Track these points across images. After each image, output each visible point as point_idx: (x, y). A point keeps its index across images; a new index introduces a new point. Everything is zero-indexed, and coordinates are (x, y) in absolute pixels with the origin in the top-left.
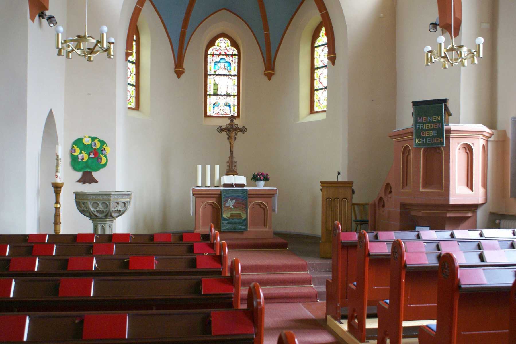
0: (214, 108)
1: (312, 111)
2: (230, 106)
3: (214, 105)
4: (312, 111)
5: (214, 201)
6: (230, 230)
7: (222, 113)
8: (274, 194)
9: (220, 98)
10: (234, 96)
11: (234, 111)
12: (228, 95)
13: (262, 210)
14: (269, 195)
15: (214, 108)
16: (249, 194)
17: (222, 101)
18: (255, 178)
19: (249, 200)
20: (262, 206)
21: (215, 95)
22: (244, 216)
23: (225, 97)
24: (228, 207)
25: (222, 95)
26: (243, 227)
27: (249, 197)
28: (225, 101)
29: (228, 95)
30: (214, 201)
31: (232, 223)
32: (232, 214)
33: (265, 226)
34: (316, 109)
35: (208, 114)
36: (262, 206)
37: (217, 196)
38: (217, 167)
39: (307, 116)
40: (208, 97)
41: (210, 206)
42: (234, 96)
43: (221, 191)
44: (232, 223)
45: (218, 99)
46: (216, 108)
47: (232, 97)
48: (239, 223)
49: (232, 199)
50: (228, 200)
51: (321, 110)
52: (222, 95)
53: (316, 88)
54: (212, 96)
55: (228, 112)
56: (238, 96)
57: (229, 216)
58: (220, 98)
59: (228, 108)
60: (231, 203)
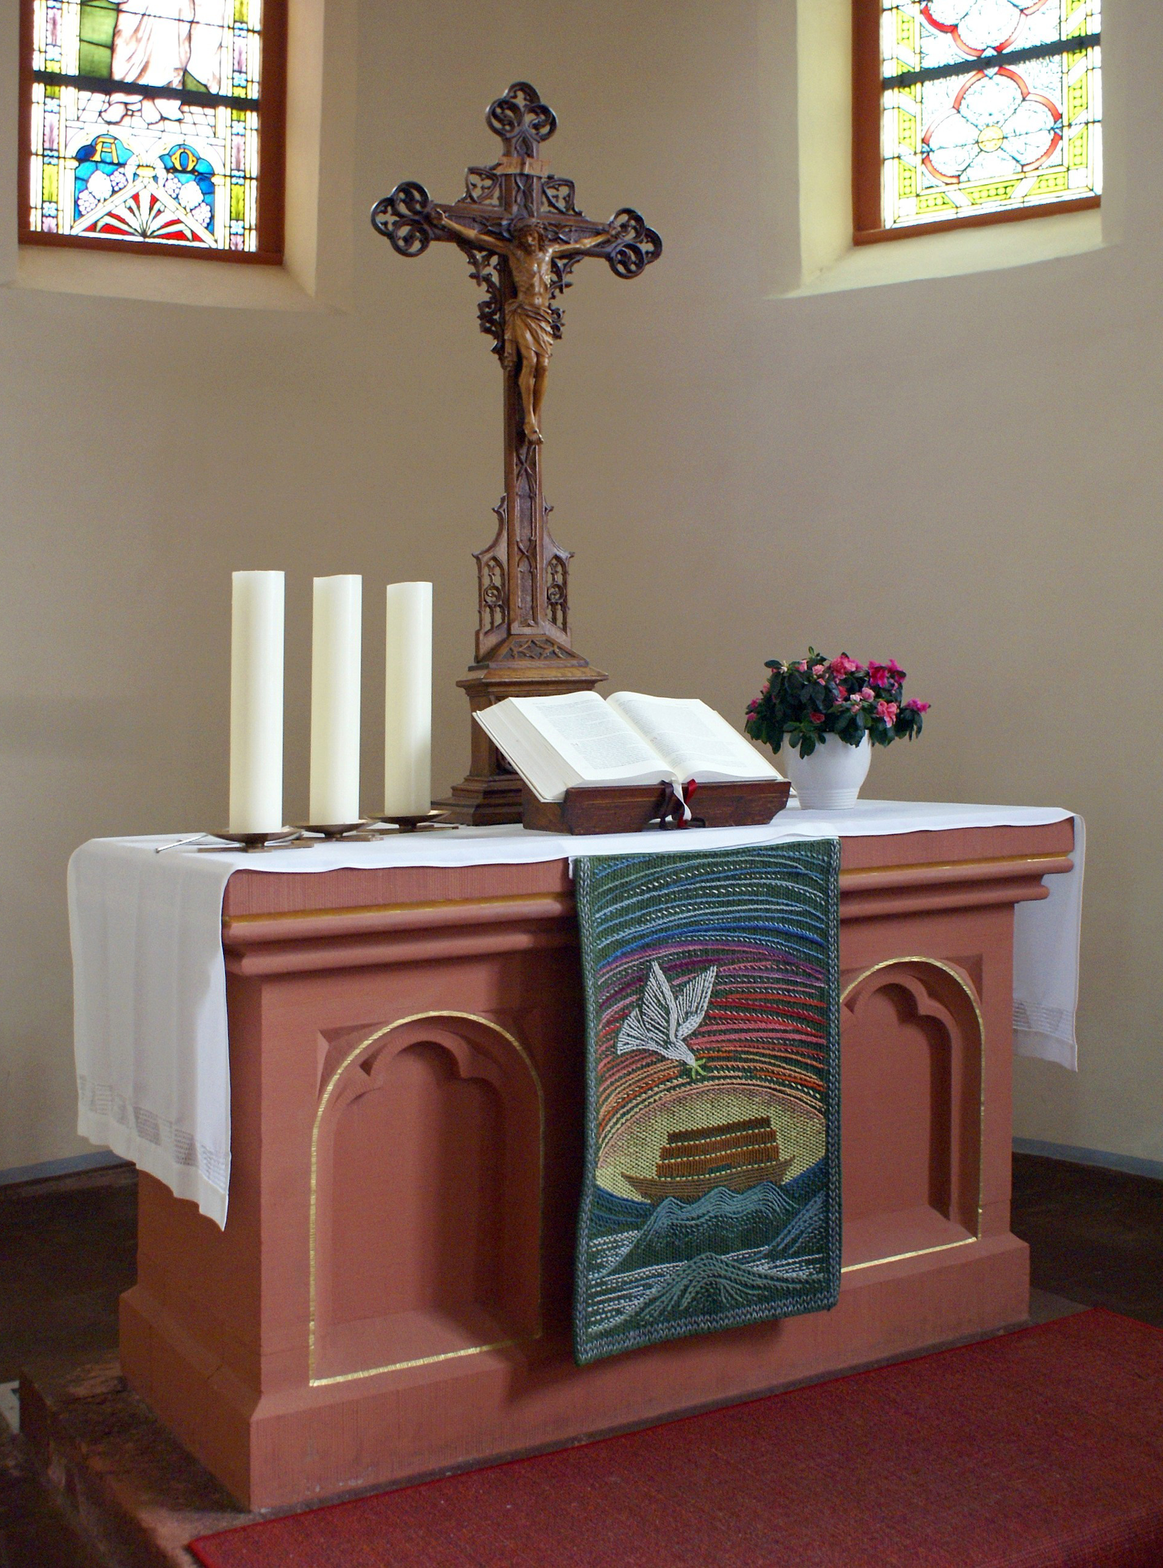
0: (82, 181)
1: (866, 226)
2: (204, 179)
3: (85, 154)
4: (866, 226)
5: (468, 999)
6: (662, 1331)
7: (140, 223)
8: (1033, 878)
9: (128, 112)
10: (238, 104)
11: (237, 217)
12: (193, 96)
13: (916, 1043)
14: (989, 888)
15: (82, 181)
16: (848, 895)
17: (148, 133)
18: (793, 711)
19: (849, 942)
20: (927, 1005)
21: (96, 81)
22: (798, 1147)
23: (170, 107)
24: (644, 1057)
25: (150, 93)
26: (795, 1271)
27: (847, 922)
28: (172, 136)
29: (193, 96)
30: (468, 999)
31: (678, 1245)
32: (681, 1143)
33: (939, 1200)
34: (896, 210)
35: (35, 222)
36: (927, 1005)
37: (520, 940)
38: (414, 605)
39: (840, 258)
40: (38, 90)
41: (416, 1072)
42: (238, 104)
43: (569, 880)
44: (678, 1245)
45: (116, 112)
46: (100, 183)
47: (223, 112)
48: (757, 1232)
49: (682, 969)
50: (639, 980)
51: (948, 214)
52: (150, 93)
53: (889, 70)
54: (68, 94)
55: (194, 223)
56: (272, 106)
57: (647, 1166)
58: (128, 112)
59: (191, 192)
60: (671, 1016)
